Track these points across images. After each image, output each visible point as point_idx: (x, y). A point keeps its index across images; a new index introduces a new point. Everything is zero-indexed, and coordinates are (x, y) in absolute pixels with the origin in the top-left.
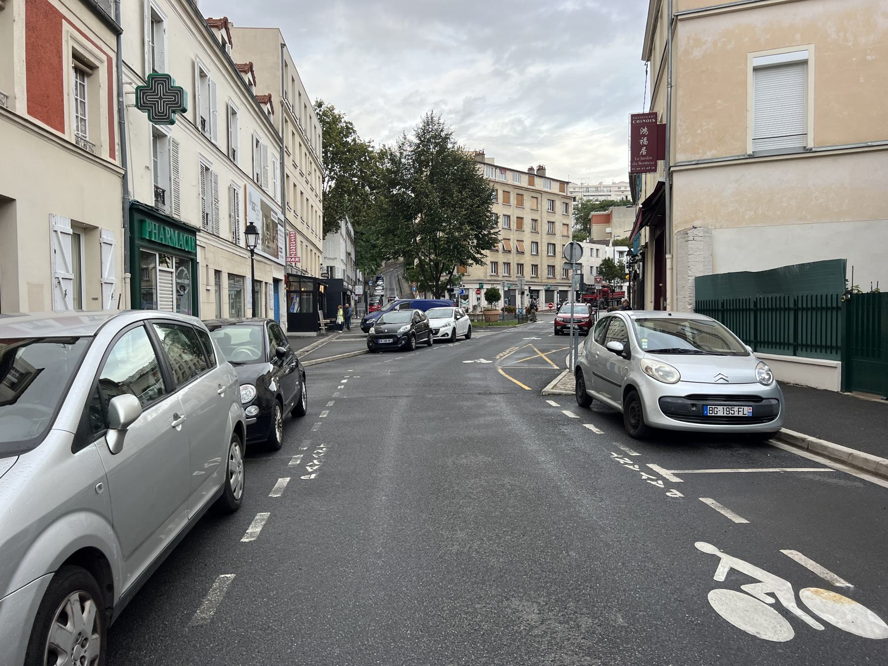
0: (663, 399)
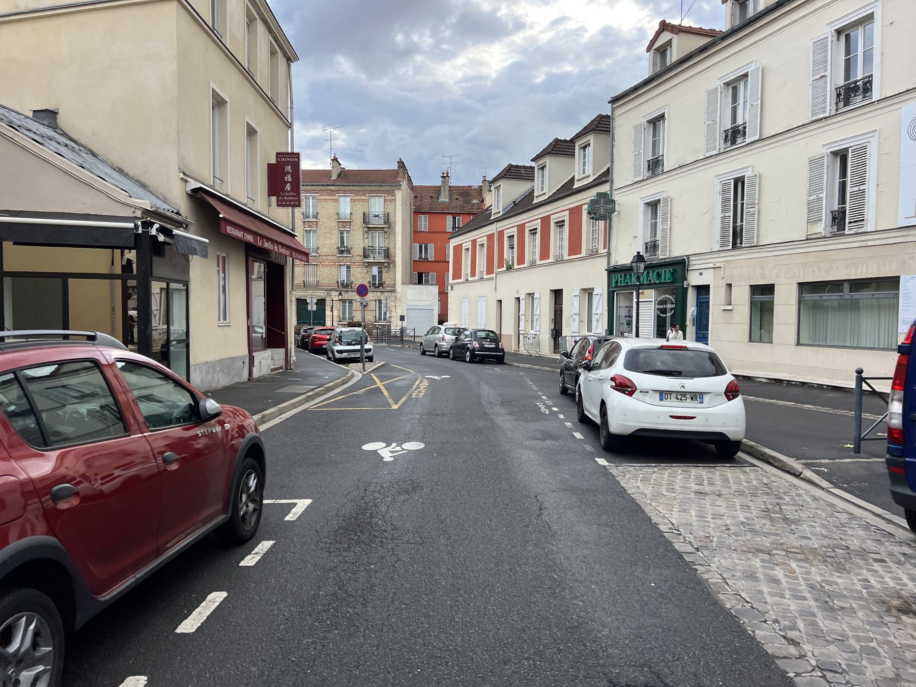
0: (404, 281)
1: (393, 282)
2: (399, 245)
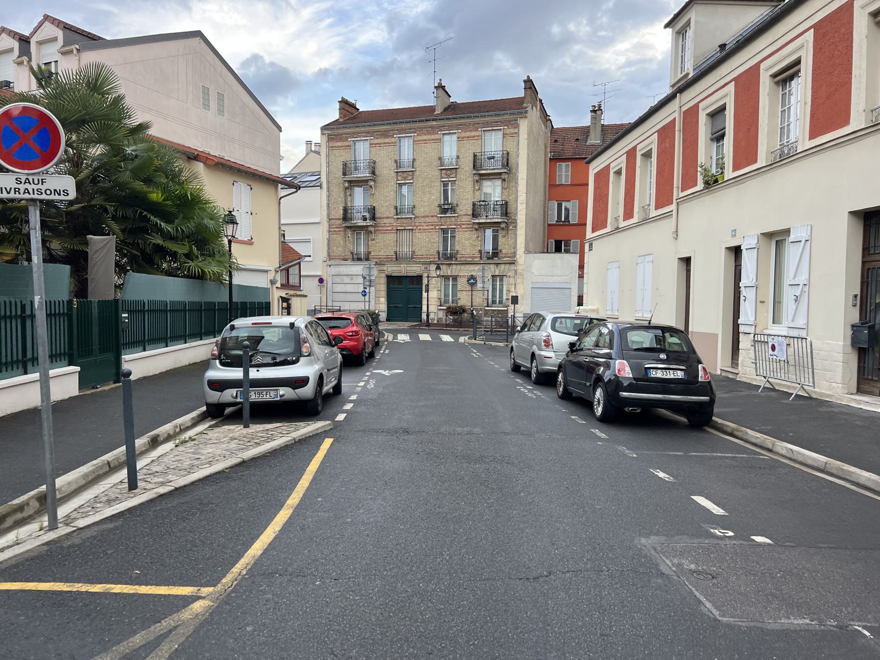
1: (513, 250)
2: (522, 197)
